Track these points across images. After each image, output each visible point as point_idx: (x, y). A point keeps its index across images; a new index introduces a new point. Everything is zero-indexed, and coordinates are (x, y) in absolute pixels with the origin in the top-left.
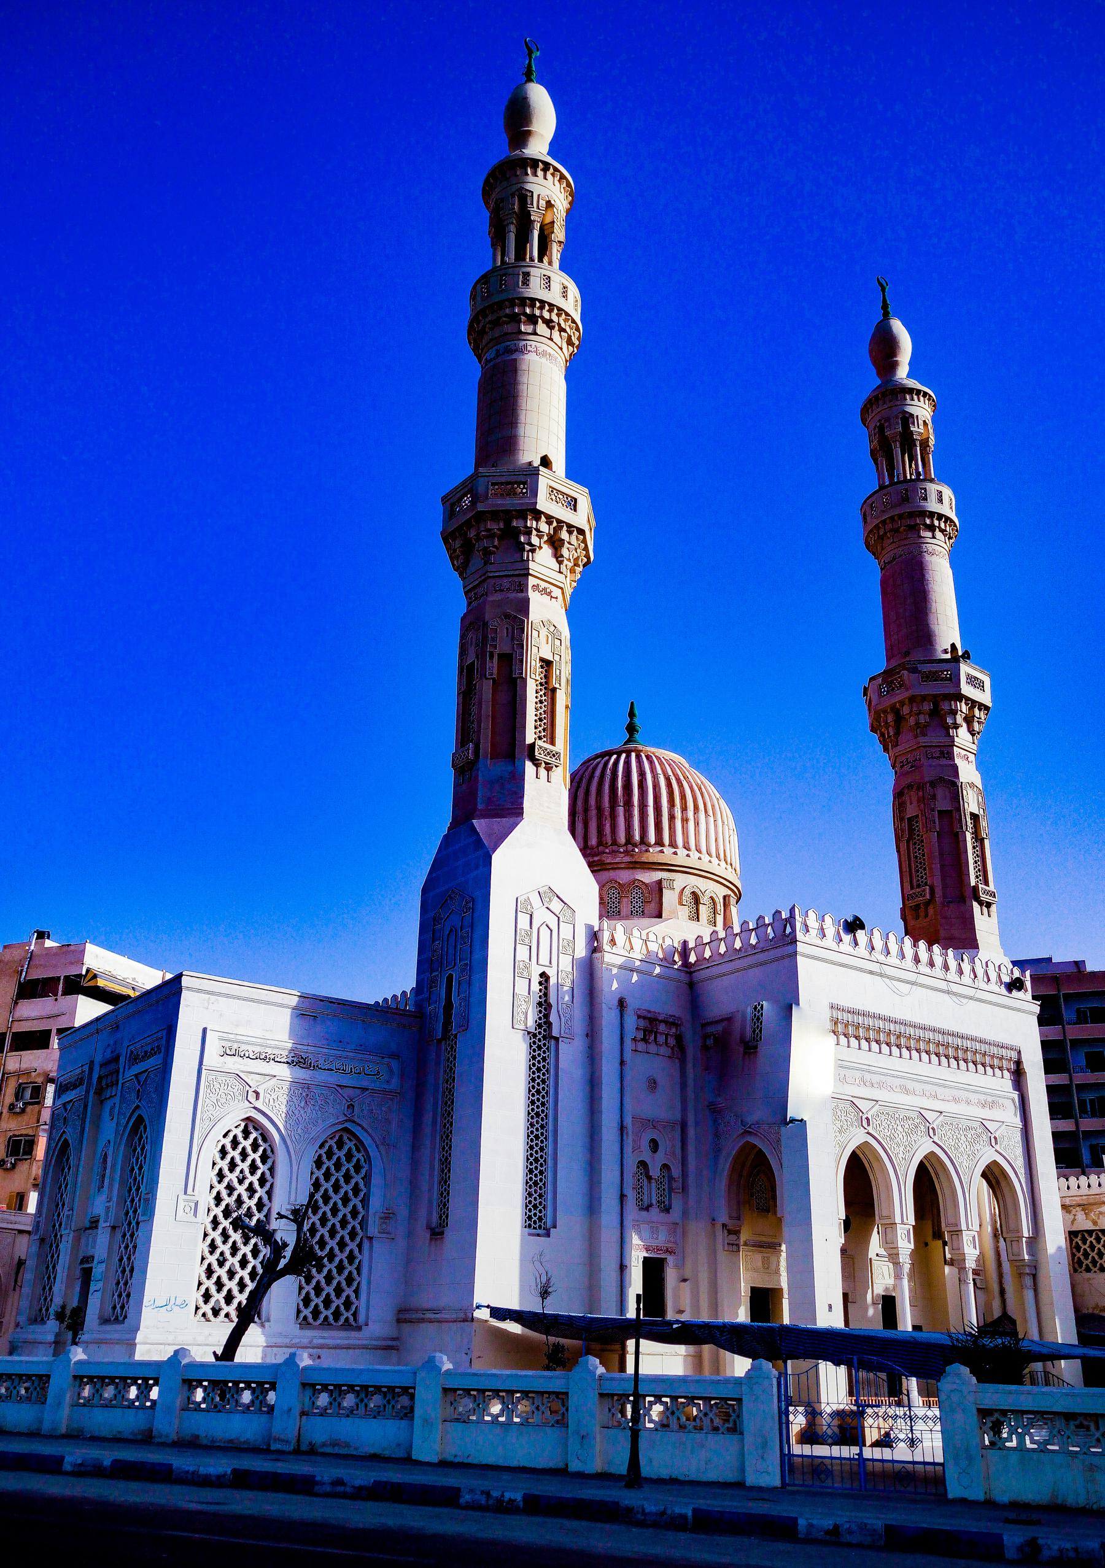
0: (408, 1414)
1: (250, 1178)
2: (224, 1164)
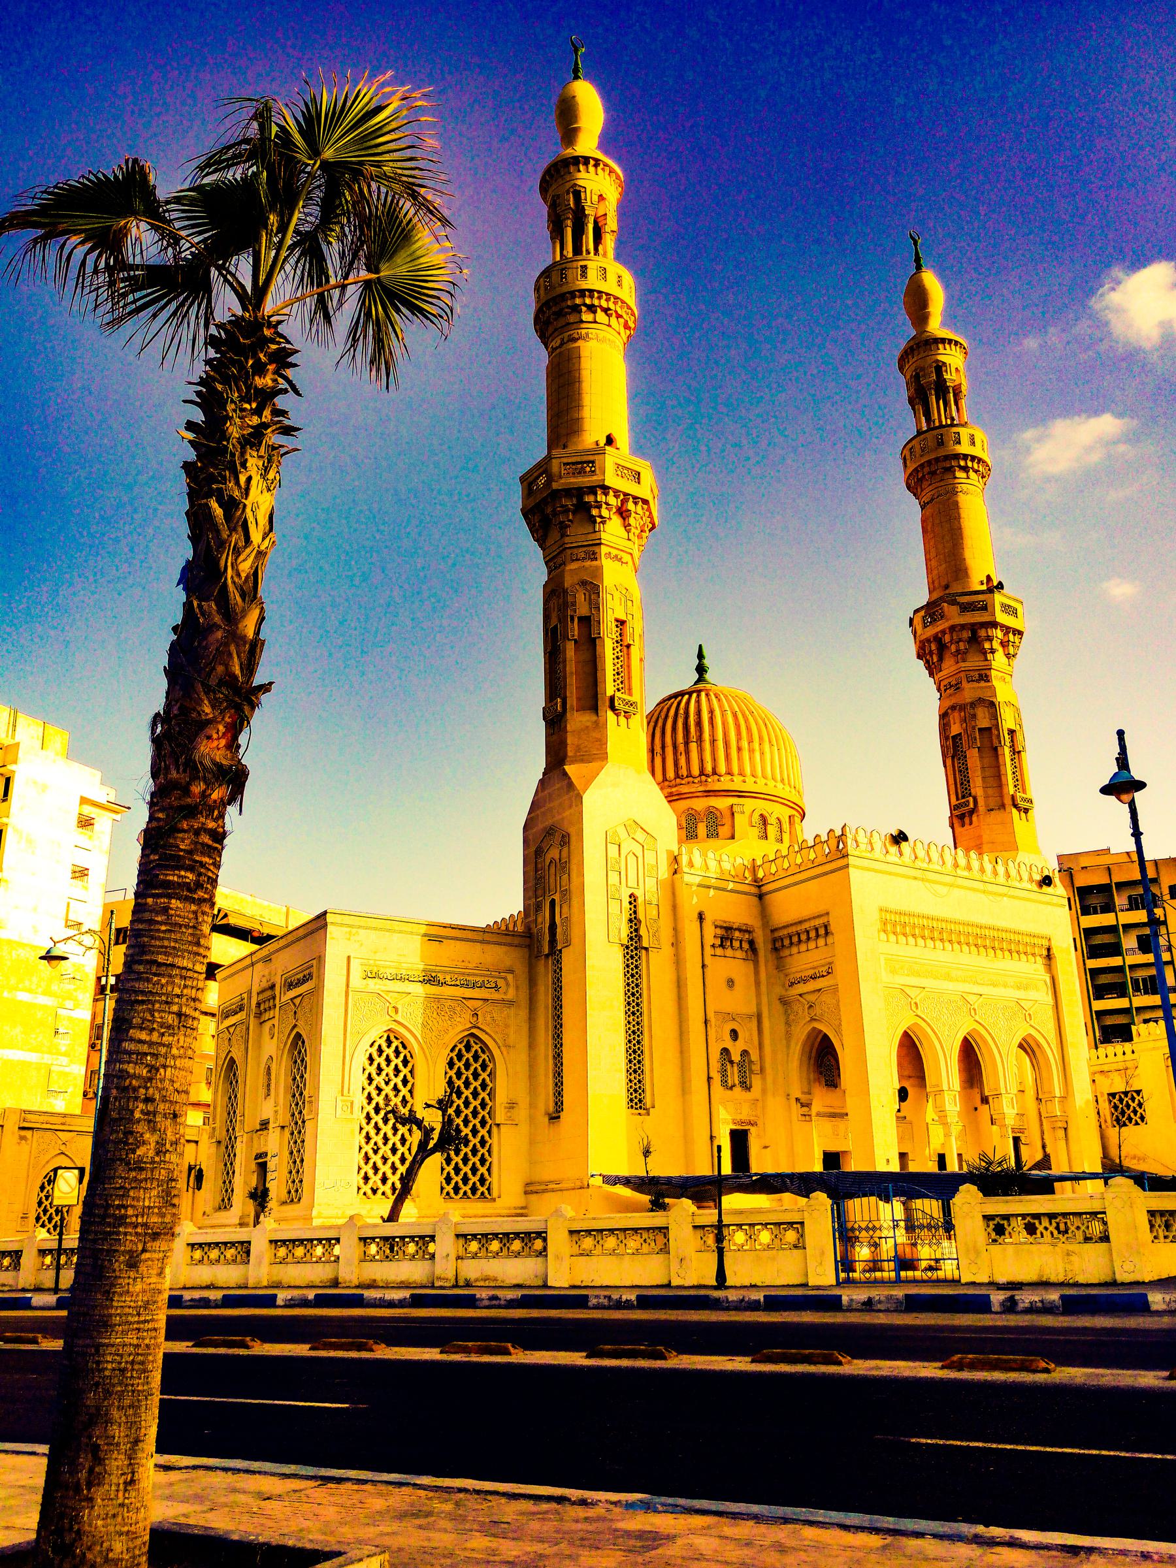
0: (543, 1253)
1: (394, 1080)
2: (373, 1070)
